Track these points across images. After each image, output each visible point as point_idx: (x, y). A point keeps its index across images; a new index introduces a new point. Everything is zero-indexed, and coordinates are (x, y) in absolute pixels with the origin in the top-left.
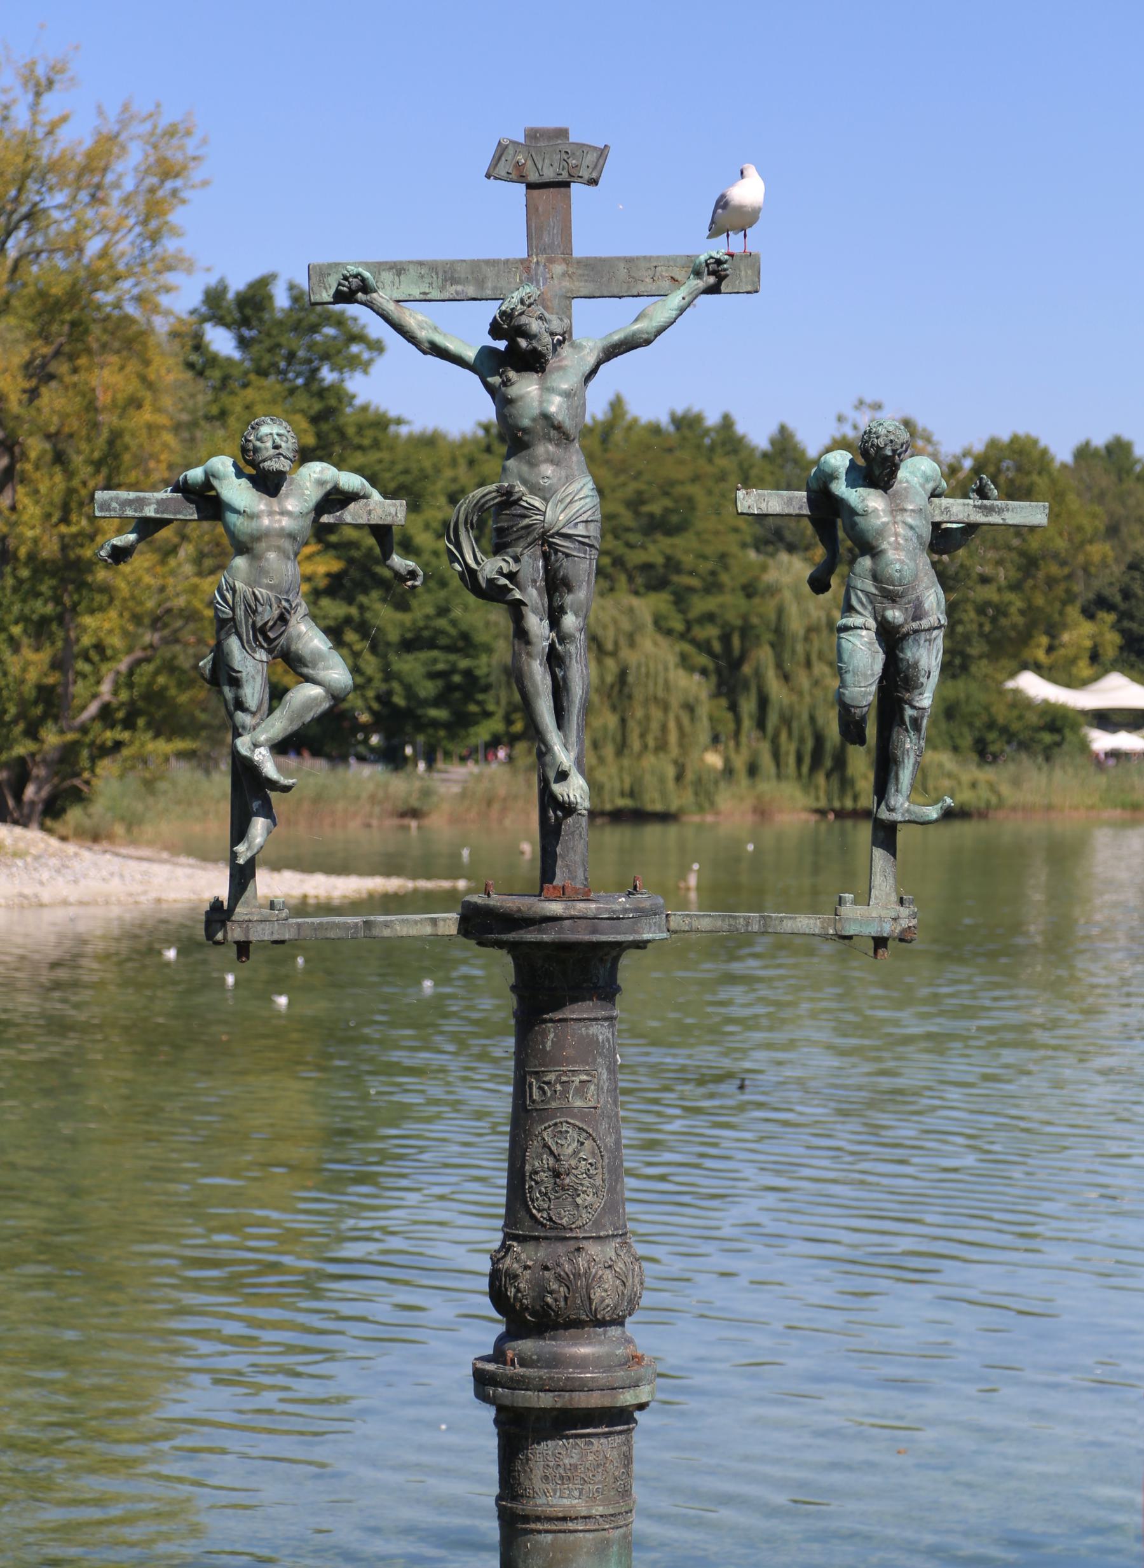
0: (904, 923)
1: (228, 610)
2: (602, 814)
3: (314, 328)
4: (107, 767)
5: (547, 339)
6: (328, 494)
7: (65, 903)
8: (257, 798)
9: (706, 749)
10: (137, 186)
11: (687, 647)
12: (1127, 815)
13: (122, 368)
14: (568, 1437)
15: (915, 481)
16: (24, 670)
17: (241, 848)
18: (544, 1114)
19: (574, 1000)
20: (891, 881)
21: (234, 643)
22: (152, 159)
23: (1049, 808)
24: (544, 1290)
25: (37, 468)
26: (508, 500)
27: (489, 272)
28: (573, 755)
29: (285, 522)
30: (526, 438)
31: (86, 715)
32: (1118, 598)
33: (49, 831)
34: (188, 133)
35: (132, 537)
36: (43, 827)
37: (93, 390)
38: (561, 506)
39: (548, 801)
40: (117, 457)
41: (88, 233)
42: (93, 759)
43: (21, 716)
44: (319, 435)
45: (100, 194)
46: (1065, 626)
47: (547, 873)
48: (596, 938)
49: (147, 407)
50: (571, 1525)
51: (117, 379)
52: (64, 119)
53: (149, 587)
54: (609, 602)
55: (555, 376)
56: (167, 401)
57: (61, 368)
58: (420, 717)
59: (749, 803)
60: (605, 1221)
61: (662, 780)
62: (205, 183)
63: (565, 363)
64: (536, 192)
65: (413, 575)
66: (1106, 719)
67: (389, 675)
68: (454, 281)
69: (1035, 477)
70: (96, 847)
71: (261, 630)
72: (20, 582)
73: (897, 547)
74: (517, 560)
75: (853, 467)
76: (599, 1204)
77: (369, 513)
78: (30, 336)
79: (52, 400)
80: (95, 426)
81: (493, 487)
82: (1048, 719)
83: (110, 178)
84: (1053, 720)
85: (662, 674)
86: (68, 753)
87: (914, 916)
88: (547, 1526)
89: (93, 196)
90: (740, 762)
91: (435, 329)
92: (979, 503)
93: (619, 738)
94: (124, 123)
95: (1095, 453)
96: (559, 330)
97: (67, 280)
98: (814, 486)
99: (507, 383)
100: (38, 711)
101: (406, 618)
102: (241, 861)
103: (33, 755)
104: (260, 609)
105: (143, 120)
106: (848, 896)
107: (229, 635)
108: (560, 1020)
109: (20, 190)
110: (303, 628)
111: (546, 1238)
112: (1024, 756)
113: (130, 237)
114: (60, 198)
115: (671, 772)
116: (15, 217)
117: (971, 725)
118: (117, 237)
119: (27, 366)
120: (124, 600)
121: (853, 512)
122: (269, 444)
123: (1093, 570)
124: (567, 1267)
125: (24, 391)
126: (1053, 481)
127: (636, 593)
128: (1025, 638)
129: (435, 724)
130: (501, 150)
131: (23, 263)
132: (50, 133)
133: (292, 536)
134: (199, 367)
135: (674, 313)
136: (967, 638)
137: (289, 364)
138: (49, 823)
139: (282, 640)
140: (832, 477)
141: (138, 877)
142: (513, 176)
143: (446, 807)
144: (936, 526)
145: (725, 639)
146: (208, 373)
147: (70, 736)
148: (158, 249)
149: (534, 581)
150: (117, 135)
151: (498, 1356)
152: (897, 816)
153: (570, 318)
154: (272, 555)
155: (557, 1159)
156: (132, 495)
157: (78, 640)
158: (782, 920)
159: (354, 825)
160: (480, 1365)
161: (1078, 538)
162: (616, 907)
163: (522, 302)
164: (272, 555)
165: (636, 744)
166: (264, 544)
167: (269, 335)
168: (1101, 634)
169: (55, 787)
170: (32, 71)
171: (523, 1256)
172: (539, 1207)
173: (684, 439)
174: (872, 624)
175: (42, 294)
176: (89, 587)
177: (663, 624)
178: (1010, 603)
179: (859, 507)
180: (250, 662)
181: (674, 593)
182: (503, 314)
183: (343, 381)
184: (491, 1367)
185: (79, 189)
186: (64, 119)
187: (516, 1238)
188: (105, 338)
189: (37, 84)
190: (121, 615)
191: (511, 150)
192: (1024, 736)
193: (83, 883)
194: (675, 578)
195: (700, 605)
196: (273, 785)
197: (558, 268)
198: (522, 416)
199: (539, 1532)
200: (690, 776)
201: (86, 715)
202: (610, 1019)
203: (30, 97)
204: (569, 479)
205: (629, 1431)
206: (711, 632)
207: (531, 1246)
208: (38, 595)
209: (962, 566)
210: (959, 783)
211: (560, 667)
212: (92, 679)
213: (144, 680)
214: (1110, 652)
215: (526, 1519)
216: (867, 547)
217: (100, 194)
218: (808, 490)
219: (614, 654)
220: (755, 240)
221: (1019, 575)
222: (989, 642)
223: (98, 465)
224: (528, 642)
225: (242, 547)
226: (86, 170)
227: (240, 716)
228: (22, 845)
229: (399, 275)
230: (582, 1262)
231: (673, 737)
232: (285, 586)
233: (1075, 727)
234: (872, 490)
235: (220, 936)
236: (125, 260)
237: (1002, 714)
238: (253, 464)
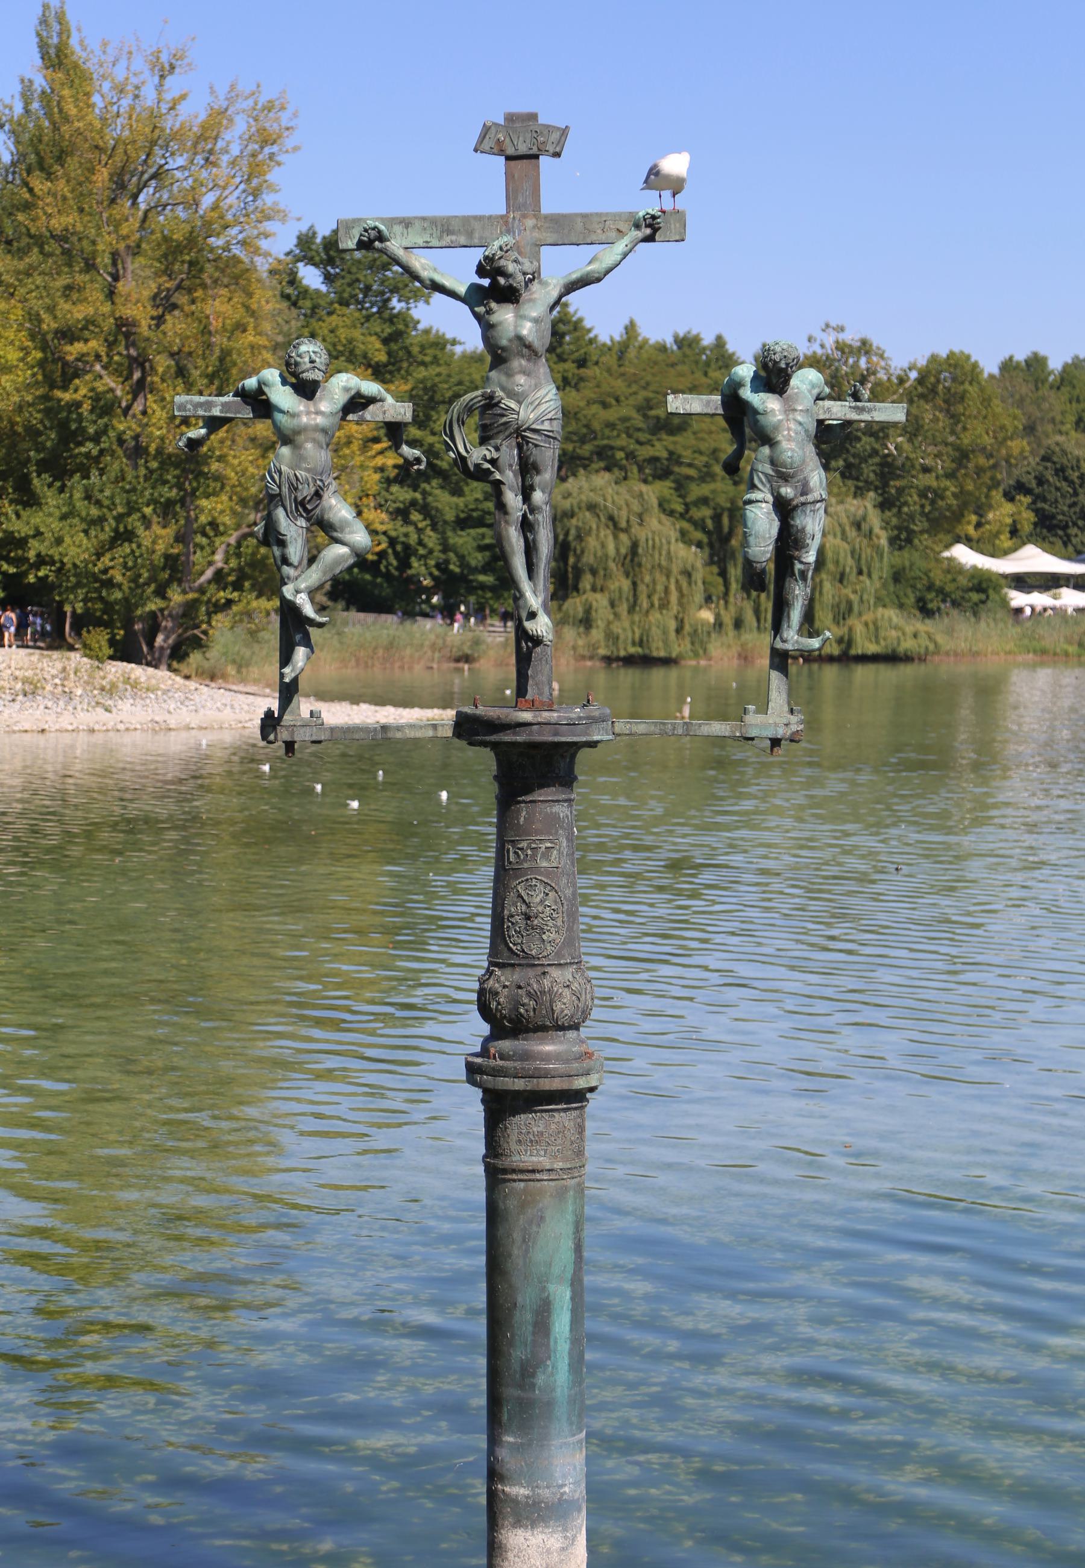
0: (794, 728)
2: (618, 659)
3: (385, 267)
4: (221, 621)
5: (520, 277)
6: (353, 398)
7: (188, 728)
9: (701, 607)
10: (242, 152)
11: (686, 525)
12: (1038, 659)
13: (230, 299)
14: (536, 1112)
15: (804, 388)
16: (154, 542)
17: (287, 670)
18: (518, 872)
19: (541, 786)
20: (784, 696)
21: (280, 513)
22: (253, 129)
23: (976, 654)
24: (518, 1003)
25: (163, 380)
26: (490, 404)
27: (477, 225)
28: (540, 600)
29: (319, 420)
31: (203, 579)
32: (1033, 484)
33: (175, 671)
34: (283, 108)
35: (203, 431)
36: (170, 668)
37: (207, 317)
38: (531, 408)
39: (522, 634)
40: (227, 371)
41: (204, 190)
42: (209, 614)
43: (152, 579)
44: (389, 354)
45: (212, 158)
46: (990, 507)
47: (521, 690)
48: (556, 739)
49: (251, 330)
50: (538, 1176)
51: (226, 308)
52: (183, 97)
53: (253, 476)
54: (622, 489)
56: (267, 326)
57: (182, 299)
58: (471, 581)
59: (735, 650)
60: (565, 952)
61: (665, 632)
62: (296, 149)
63: (535, 296)
64: (512, 163)
65: (418, 461)
66: (1023, 582)
67: (446, 548)
68: (449, 232)
69: (967, 386)
70: (213, 685)
71: (302, 503)
72: (151, 472)
73: (789, 439)
74: (497, 449)
75: (756, 377)
76: (560, 939)
78: (157, 274)
79: (175, 324)
80: (209, 346)
81: (479, 392)
82: (976, 581)
83: (220, 144)
84: (980, 583)
85: (665, 547)
86: (190, 609)
87: (801, 722)
88: (520, 1177)
89: (207, 160)
90: (728, 619)
91: (435, 270)
93: (631, 599)
94: (231, 100)
95: (1017, 366)
96: (530, 271)
97: (187, 228)
98: (727, 392)
99: (489, 312)
100: (165, 575)
101: (460, 501)
102: (287, 680)
103: (162, 610)
105: (246, 98)
106: (751, 707)
107: (276, 507)
109: (148, 155)
110: (333, 501)
111: (520, 965)
112: (955, 612)
113: (236, 193)
114: (180, 161)
115: (672, 625)
116: (146, 176)
117: (913, 587)
118: (227, 192)
119: (155, 297)
120: (234, 486)
121: (756, 412)
122: (307, 360)
123: (1013, 461)
125: (152, 318)
126: (982, 389)
127: (645, 481)
128: (958, 517)
129: (483, 587)
130: (486, 130)
131: (150, 215)
132: (172, 108)
133: (324, 431)
134: (294, 298)
135: (619, 257)
136: (911, 517)
137: (365, 296)
138: (175, 664)
139: (318, 511)
141: (246, 707)
142: (495, 151)
143: (492, 653)
144: (820, 422)
145: (717, 518)
146: (301, 303)
147: (191, 596)
148: (259, 203)
149: (511, 466)
150: (226, 109)
151: (484, 1053)
152: (789, 646)
153: (539, 261)
154: (309, 446)
155: (528, 906)
157: (197, 518)
159: (418, 668)
160: (470, 1059)
161: (1001, 436)
162: (573, 716)
163: (501, 248)
164: (309, 446)
165: (645, 604)
167: (349, 272)
168: (1020, 513)
169: (179, 636)
170: (158, 58)
172: (515, 942)
173: (685, 356)
175: (166, 239)
176: (205, 475)
177: (666, 506)
178: (946, 489)
180: (293, 528)
181: (675, 481)
182: (486, 258)
183: (408, 309)
184: (479, 1060)
185: (195, 154)
186: (183, 97)
187: (497, 965)
188: (217, 274)
189: (162, 69)
190: (231, 499)
191: (493, 130)
192: (957, 595)
193: (202, 711)
194: (676, 469)
195: (696, 491)
196: (312, 622)
197: (530, 222)
199: (514, 1181)
200: (687, 628)
201: (203, 579)
202: (569, 801)
203: (156, 79)
204: (537, 387)
205: (582, 1107)
206: (706, 512)
207: (508, 971)
208: (165, 482)
209: (907, 458)
210: (904, 634)
212: (208, 550)
213: (250, 551)
214: (1026, 528)
215: (505, 1171)
216: (766, 439)
217: (212, 158)
218: (723, 395)
219: (626, 530)
220: (682, 202)
221: (954, 465)
222: (928, 520)
223: (211, 378)
224: (506, 513)
225: (287, 439)
226: (200, 138)
227: (286, 570)
228: (153, 682)
229: (407, 227)
230: (546, 982)
231: (674, 597)
232: (319, 469)
233: (997, 588)
235: (272, 737)
236: (233, 210)
237: (938, 577)
238: (294, 374)
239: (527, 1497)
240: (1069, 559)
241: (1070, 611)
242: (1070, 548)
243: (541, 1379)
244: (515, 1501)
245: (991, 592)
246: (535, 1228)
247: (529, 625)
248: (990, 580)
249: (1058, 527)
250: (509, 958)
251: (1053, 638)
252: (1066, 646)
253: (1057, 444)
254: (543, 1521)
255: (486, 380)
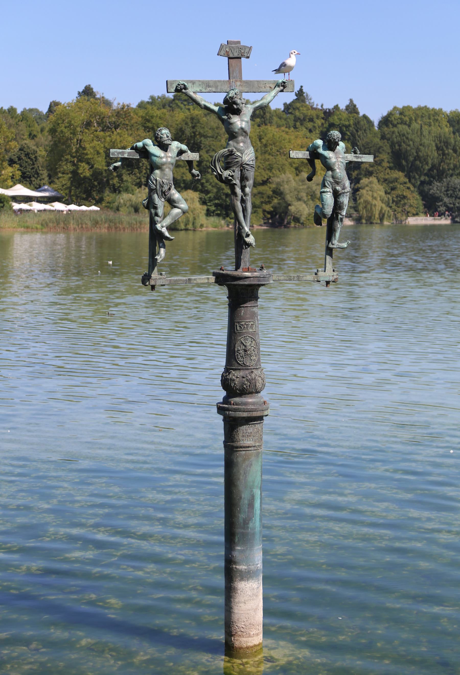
1: (154, 186)
8: (161, 243)
12: (26, 230)
14: (249, 425)
19: (250, 301)
21: (156, 196)
26: (231, 153)
27: (219, 84)
29: (169, 160)
30: (236, 135)
50: (250, 449)
55: (243, 116)
63: (244, 112)
64: (231, 60)
66: (16, 199)
68: (209, 86)
77: (189, 157)
88: (244, 449)
92: (355, 155)
98: (311, 150)
104: (164, 186)
107: (154, 194)
108: (246, 307)
122: (165, 136)
124: (249, 377)
139: (168, 195)
140: (318, 147)
152: (335, 246)
154: (167, 170)
155: (245, 346)
156: (121, 151)
158: (303, 276)
161: (7, 140)
164: (167, 170)
166: (165, 166)
168: (15, 171)
171: (236, 375)
174: (332, 191)
179: (328, 156)
180: (160, 202)
191: (225, 47)
196: (167, 239)
197: (238, 83)
198: (235, 128)
199: (241, 451)
204: (248, 148)
211: (244, 203)
215: (237, 447)
229: (193, 84)
230: (253, 375)
233: (8, 202)
234: (330, 152)
239: (246, 569)
240: (33, 190)
241: (36, 211)
242: (32, 186)
243: (251, 525)
244: (241, 571)
245: (5, 203)
246: (249, 469)
247: (247, 239)
248: (4, 198)
249: (27, 177)
250: (238, 367)
251: (30, 221)
252: (36, 225)
253: (26, 144)
254: (252, 578)
255: (228, 144)
